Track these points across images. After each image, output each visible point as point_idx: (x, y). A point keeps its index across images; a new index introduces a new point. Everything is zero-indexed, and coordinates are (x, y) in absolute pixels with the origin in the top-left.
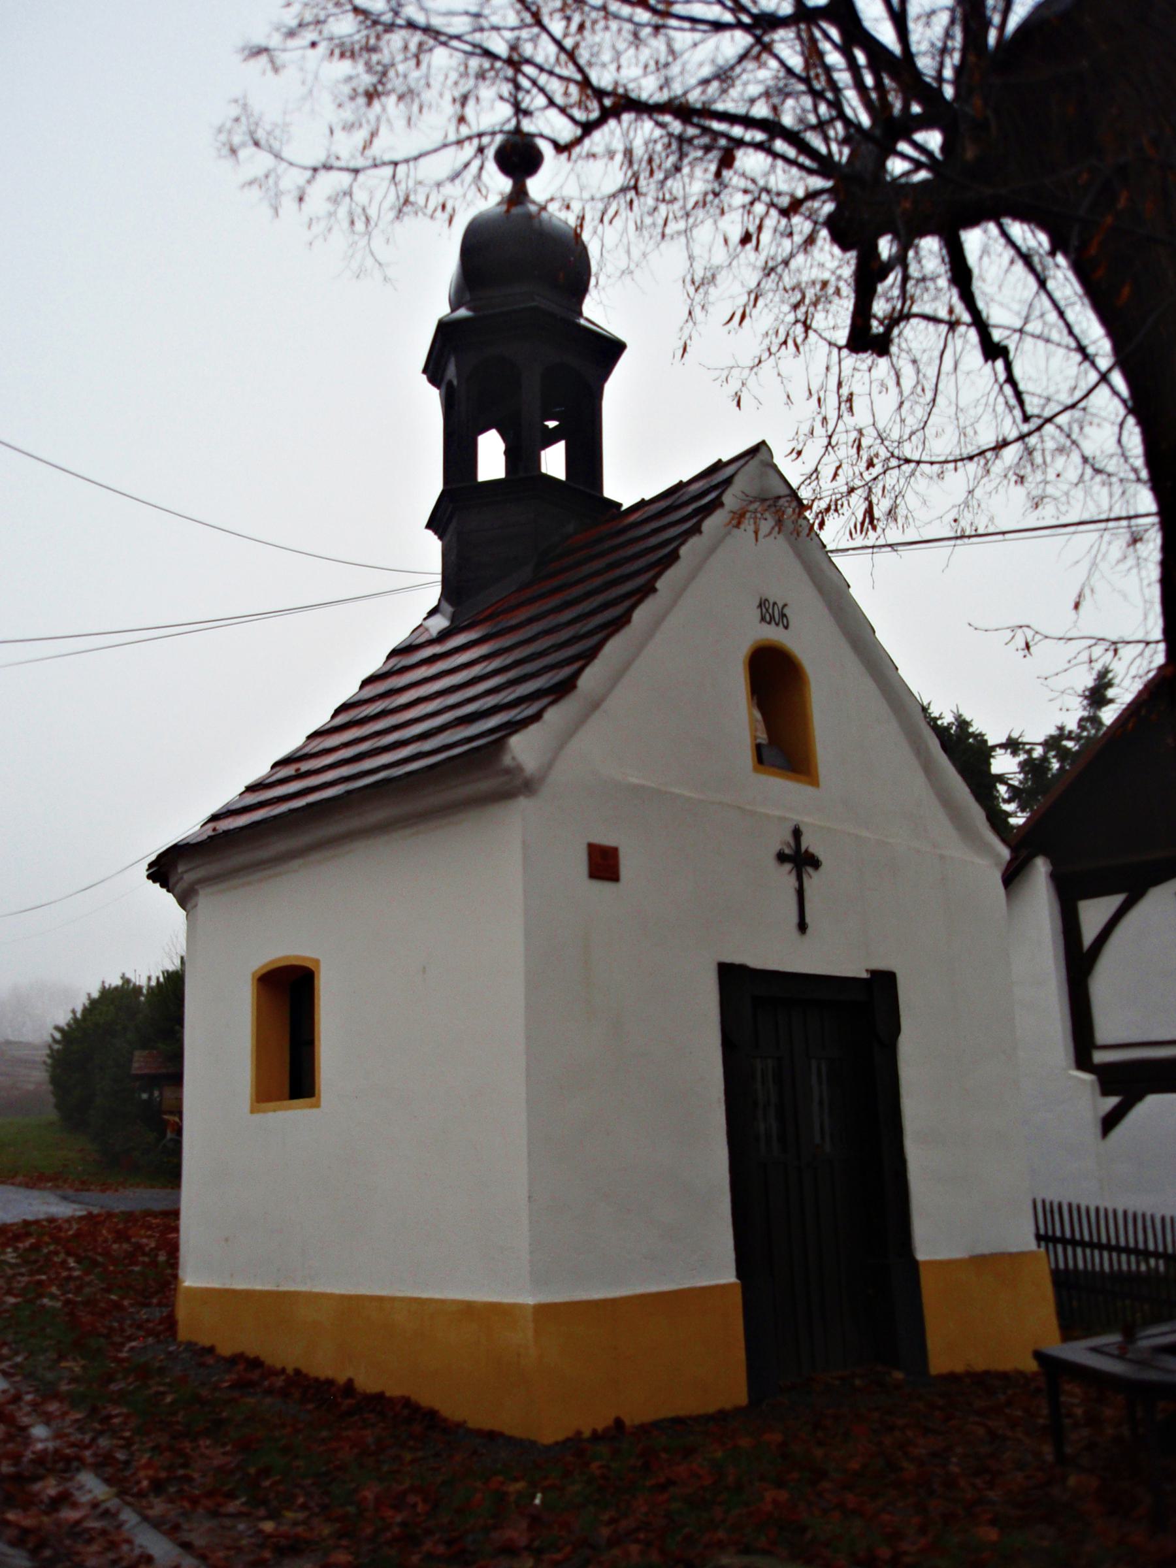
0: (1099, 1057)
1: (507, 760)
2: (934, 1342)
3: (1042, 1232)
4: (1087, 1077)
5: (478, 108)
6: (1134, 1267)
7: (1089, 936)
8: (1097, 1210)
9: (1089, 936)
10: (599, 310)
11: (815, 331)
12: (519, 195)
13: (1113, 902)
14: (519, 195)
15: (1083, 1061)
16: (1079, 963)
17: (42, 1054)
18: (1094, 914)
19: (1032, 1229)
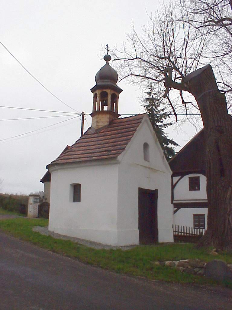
0: (174, 202)
1: (117, 159)
2: (159, 239)
3: (175, 230)
4: (172, 205)
5: (113, 58)
6: (179, 234)
7: (174, 183)
8: (177, 226)
9: (174, 183)
10: (119, 84)
11: (173, 115)
12: (107, 64)
13: (179, 178)
14: (107, 64)
15: (172, 203)
16: (173, 187)
17: (52, 173)
18: (176, 179)
19: (173, 230)
